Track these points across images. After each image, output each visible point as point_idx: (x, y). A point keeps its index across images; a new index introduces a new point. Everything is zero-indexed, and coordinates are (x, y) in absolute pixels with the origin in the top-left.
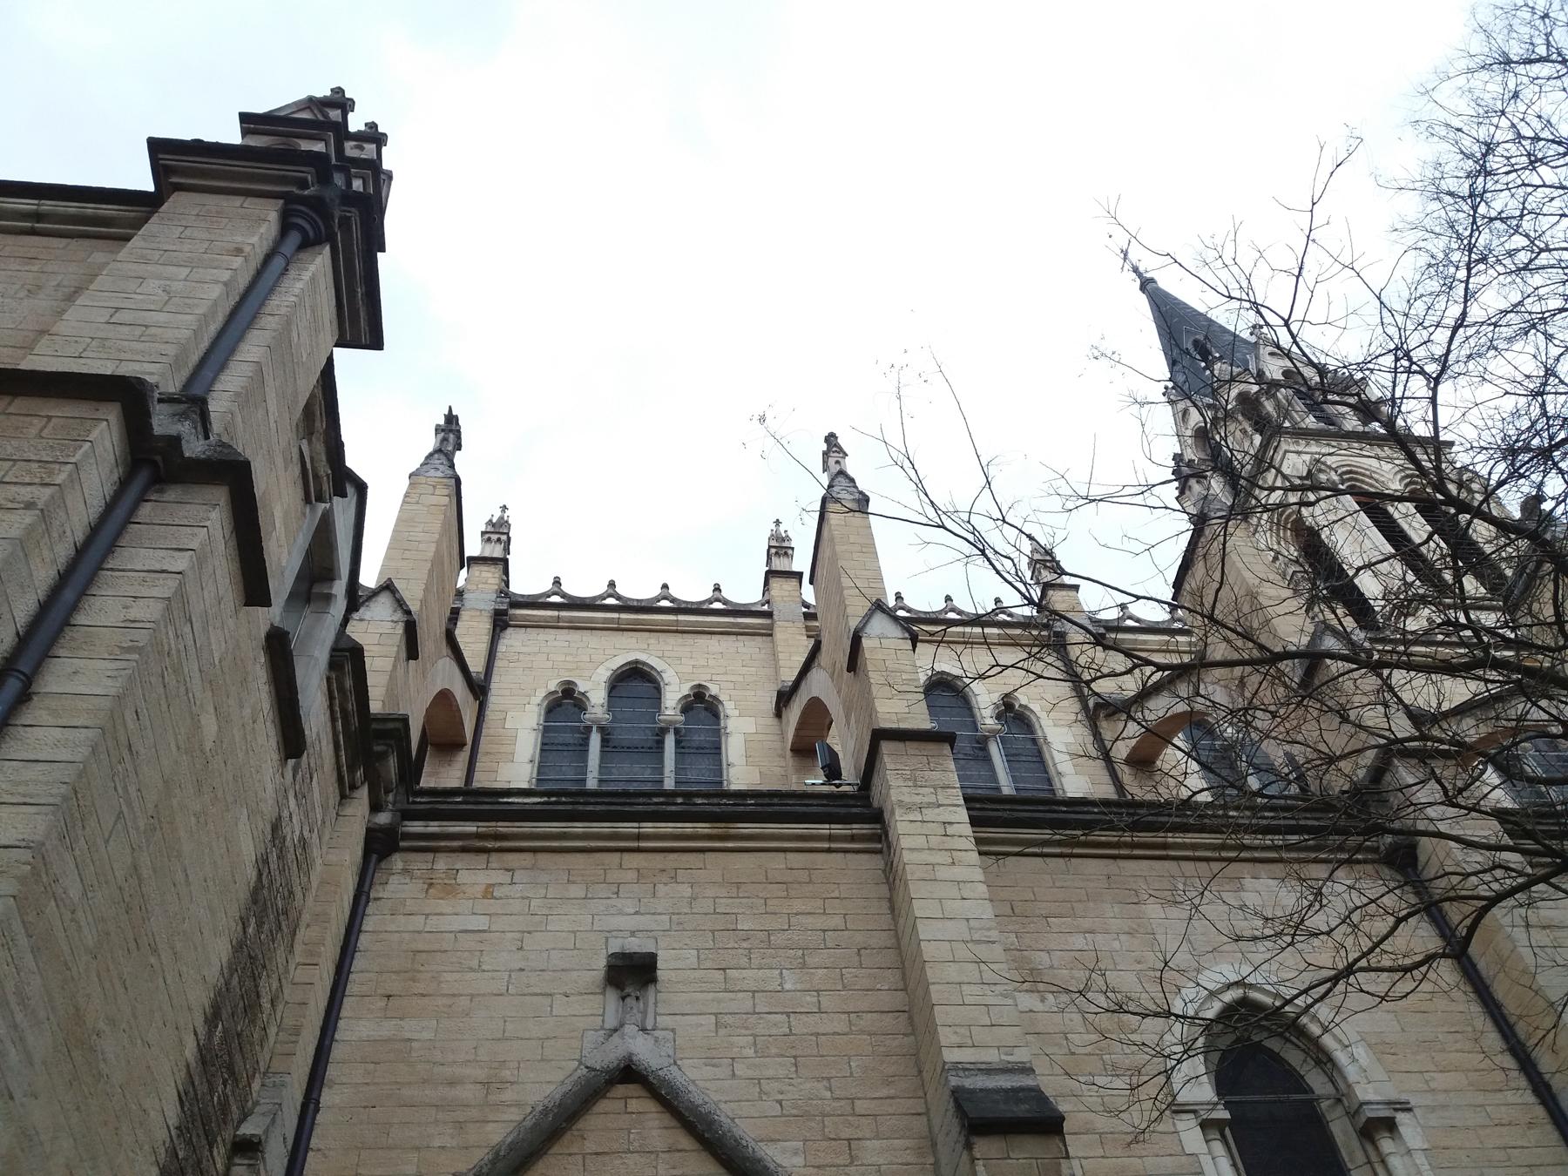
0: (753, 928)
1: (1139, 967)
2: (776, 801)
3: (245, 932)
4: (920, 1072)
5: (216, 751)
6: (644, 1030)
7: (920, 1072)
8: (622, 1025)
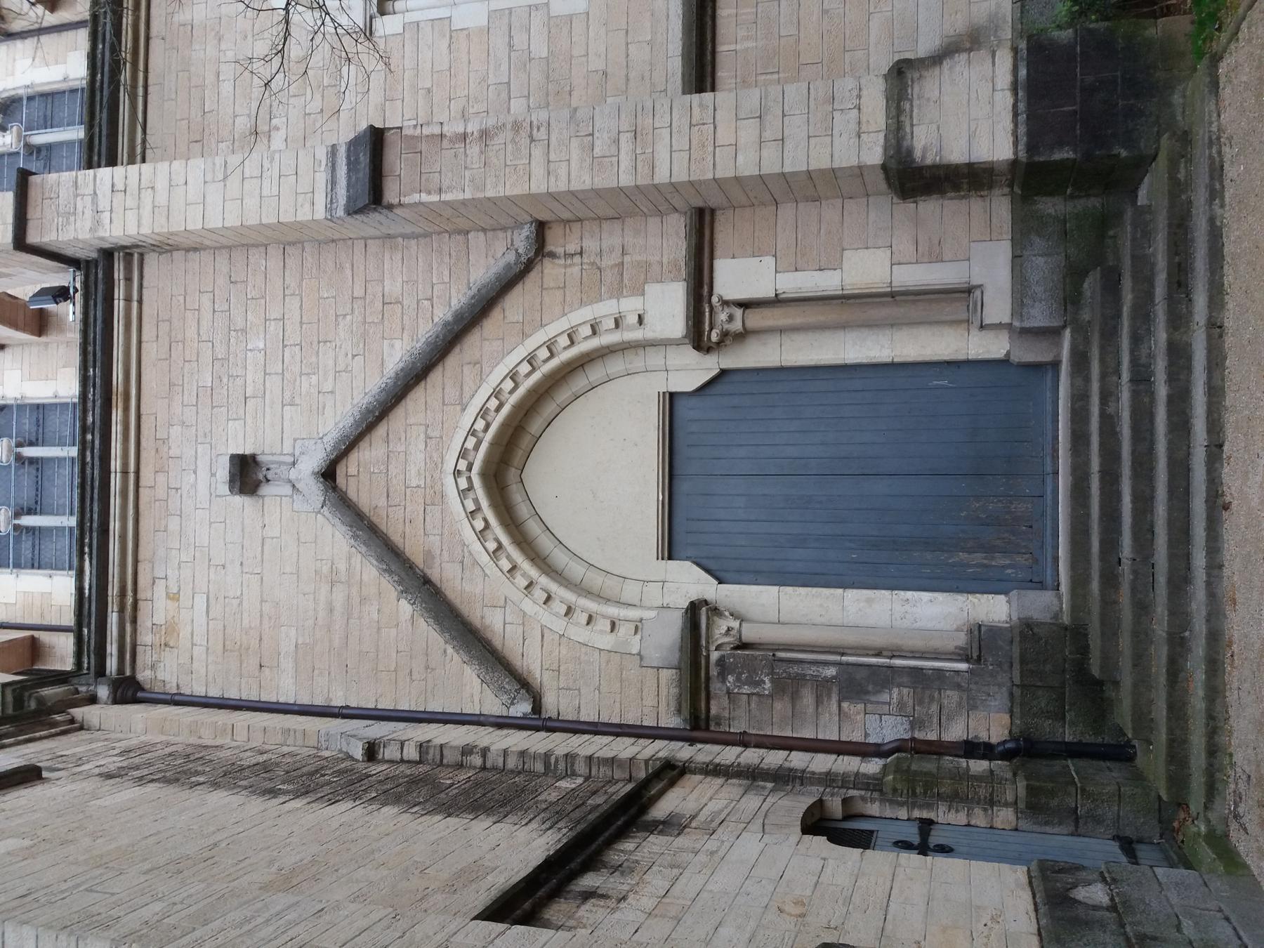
0: (210, 373)
1: (250, 36)
2: (90, 349)
3: (204, 783)
4: (333, 241)
5: (33, 835)
6: (294, 464)
7: (333, 241)
8: (290, 481)
